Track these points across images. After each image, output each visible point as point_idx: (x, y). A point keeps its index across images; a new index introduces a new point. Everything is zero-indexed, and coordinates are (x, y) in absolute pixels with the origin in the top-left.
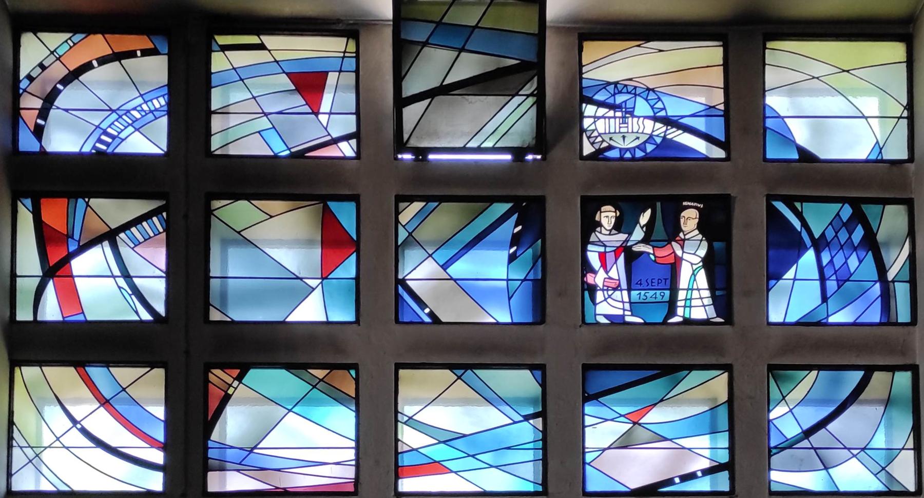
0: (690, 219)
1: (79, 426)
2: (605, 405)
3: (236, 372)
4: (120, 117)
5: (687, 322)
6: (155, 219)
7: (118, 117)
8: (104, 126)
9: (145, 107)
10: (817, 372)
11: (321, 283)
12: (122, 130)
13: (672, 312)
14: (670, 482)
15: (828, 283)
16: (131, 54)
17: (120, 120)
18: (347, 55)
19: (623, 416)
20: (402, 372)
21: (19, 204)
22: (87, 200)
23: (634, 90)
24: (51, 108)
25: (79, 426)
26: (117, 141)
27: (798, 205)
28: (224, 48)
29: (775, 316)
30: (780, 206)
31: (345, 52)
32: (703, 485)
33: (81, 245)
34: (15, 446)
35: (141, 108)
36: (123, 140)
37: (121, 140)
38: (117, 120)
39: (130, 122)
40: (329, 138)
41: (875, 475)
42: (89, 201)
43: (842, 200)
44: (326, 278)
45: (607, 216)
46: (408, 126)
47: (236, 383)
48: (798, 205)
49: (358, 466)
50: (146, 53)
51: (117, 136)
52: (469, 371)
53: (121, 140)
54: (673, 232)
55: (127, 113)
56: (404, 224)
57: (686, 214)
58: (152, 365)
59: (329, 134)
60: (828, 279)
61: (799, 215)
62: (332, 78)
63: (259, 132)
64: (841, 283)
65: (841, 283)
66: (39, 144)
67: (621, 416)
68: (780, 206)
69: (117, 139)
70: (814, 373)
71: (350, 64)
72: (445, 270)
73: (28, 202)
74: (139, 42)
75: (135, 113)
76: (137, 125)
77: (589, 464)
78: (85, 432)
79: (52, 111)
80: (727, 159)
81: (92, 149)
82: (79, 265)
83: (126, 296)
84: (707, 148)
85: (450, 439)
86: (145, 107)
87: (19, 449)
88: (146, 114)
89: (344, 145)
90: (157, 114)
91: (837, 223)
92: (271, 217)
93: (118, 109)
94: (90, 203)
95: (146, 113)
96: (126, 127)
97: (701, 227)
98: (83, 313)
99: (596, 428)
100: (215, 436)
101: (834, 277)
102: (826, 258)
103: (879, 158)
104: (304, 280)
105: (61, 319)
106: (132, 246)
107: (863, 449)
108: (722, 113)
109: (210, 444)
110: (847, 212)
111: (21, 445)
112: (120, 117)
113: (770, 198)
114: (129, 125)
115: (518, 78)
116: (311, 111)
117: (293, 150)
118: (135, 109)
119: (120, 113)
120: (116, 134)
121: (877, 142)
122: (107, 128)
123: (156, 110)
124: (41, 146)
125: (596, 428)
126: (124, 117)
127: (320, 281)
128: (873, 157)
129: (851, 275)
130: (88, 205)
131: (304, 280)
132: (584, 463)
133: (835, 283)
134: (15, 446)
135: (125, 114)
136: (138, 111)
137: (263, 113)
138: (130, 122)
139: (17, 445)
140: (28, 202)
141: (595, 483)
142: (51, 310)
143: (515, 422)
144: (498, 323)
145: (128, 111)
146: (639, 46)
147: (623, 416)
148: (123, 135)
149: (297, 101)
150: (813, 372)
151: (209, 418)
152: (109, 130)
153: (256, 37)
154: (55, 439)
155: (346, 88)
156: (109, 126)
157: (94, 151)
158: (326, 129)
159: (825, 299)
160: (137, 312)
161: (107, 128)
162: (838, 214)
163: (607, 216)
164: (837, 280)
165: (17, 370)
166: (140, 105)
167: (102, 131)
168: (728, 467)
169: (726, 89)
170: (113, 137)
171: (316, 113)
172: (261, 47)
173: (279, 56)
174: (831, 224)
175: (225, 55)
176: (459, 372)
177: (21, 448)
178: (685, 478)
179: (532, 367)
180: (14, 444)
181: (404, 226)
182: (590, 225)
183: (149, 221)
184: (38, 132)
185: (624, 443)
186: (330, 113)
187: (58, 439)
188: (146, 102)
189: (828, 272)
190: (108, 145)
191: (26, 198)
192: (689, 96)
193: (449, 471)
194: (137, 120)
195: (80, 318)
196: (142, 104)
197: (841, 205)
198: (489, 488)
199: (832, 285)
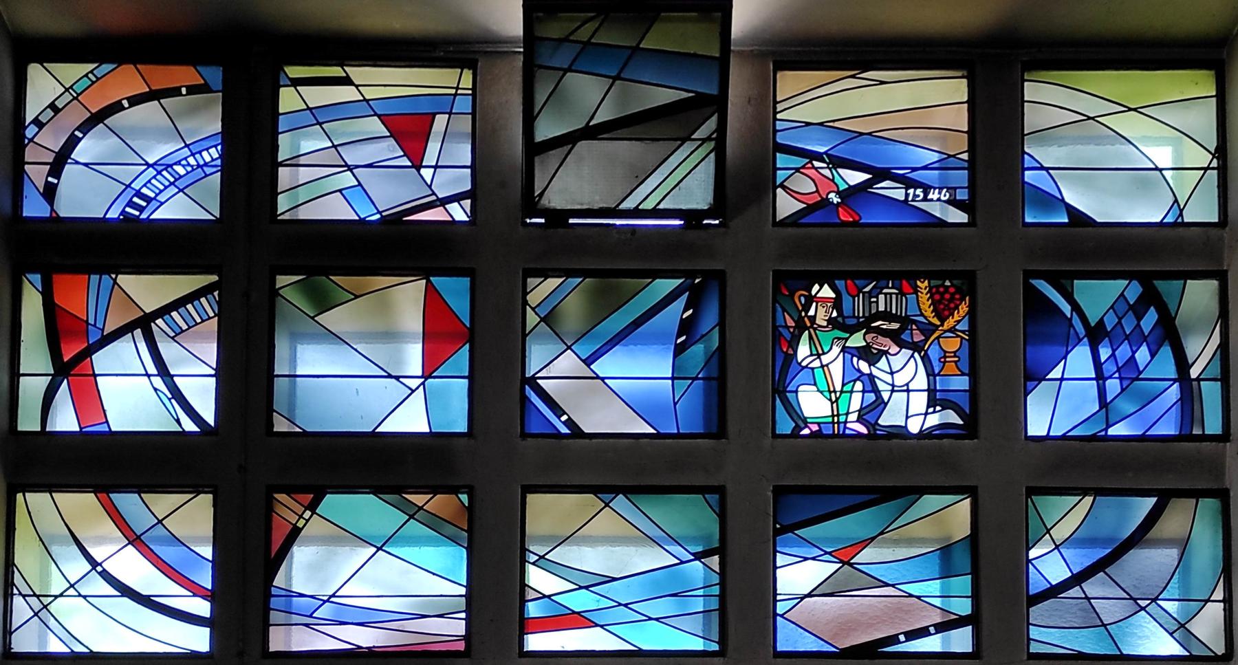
1: (99, 569)
11: (423, 384)
12: (161, 191)
16: (175, 92)
18: (453, 91)
19: (830, 553)
20: (532, 498)
22: (114, 276)
25: (99, 569)
26: (154, 204)
29: (1037, 426)
32: (932, 644)
33: (105, 334)
34: (15, 594)
36: (162, 204)
37: (343, 192)
40: (434, 198)
41: (1171, 634)
44: (430, 377)
47: (308, 514)
53: (343, 192)
59: (434, 194)
62: (440, 121)
63: (340, 191)
74: (186, 75)
76: (179, 183)
77: (782, 616)
78: (107, 576)
81: (121, 214)
87: (21, 598)
88: (193, 170)
90: (208, 170)
93: (155, 163)
96: (166, 187)
98: (107, 422)
100: (279, 581)
106: (172, 334)
109: (274, 591)
111: (23, 593)
118: (178, 163)
120: (152, 195)
121: (1176, 201)
123: (206, 164)
128: (1169, 219)
132: (775, 615)
134: (15, 594)
135: (166, 169)
136: (183, 166)
137: (346, 165)
139: (17, 593)
141: (789, 639)
145: (171, 166)
147: (830, 553)
148: (162, 198)
149: (389, 150)
151: (273, 556)
152: (144, 191)
153: (340, 68)
155: (459, 136)
160: (178, 421)
165: (20, 496)
166: (185, 159)
170: (148, 200)
171: (418, 166)
176: (607, 497)
177: (24, 596)
181: (533, 309)
186: (436, 167)
188: (193, 155)
194: (181, 177)
195: (104, 428)
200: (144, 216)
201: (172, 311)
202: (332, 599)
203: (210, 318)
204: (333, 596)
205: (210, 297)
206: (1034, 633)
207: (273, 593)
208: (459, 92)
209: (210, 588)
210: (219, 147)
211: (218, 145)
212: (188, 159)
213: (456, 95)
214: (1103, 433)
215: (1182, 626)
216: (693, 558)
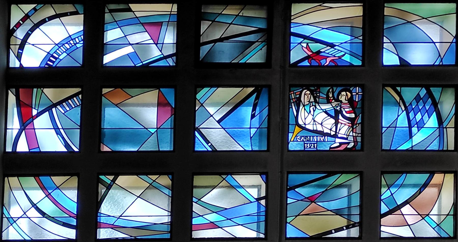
4: (60, 47)
6: (75, 98)
7: (58, 47)
8: (51, 53)
9: (72, 42)
10: (405, 174)
11: (157, 131)
12: (60, 55)
14: (330, 232)
15: (413, 129)
16: (65, 15)
17: (59, 49)
18: (169, 13)
21: (9, 91)
23: (441, 62)
24: (25, 44)
26: (58, 60)
27: (398, 89)
28: (111, 11)
31: (171, 12)
34: (4, 218)
35: (70, 42)
38: (58, 49)
39: (65, 50)
40: (162, 56)
41: (434, 229)
42: (43, 90)
43: (421, 86)
48: (398, 89)
50: (72, 14)
51: (58, 58)
52: (229, 176)
55: (63, 45)
56: (199, 99)
58: (72, 175)
59: (162, 54)
60: (413, 127)
61: (399, 94)
65: (420, 128)
66: (19, 63)
67: (306, 198)
69: (58, 59)
70: (404, 175)
72: (219, 123)
73: (14, 90)
74: (69, 8)
75: (67, 45)
77: (289, 223)
79: (26, 46)
81: (46, 65)
82: (37, 123)
83: (60, 139)
84: (350, 59)
85: (219, 211)
86: (72, 42)
87: (6, 219)
88: (72, 46)
89: (170, 60)
91: (418, 98)
92: (132, 97)
93: (58, 44)
94: (44, 91)
95: (72, 45)
98: (39, 147)
101: (416, 126)
102: (411, 115)
103: (441, 64)
104: (148, 129)
105: (28, 150)
107: (428, 215)
108: (361, 41)
112: (60, 47)
114: (64, 52)
116: (153, 43)
117: (144, 63)
119: (60, 45)
121: (440, 55)
122: (53, 53)
124: (21, 64)
126: (62, 47)
127: (156, 129)
128: (437, 63)
129: (425, 124)
130: (42, 92)
131: (148, 129)
132: (286, 223)
133: (416, 129)
134: (4, 218)
135: (62, 46)
136: (68, 44)
138: (65, 50)
140: (14, 90)
142: (23, 147)
143: (251, 202)
144: (245, 151)
145: (64, 44)
146: (320, 5)
150: (404, 174)
151: (99, 201)
152: (55, 55)
154: (24, 213)
156: (54, 53)
157: (46, 66)
158: (161, 51)
161: (53, 53)
162: (418, 94)
164: (418, 127)
165: (6, 178)
167: (51, 55)
172: (130, 10)
173: (138, 14)
174: (415, 98)
175: (323, 129)
176: (224, 177)
177: (7, 218)
179: (261, 174)
180: (4, 216)
181: (199, 101)
183: (72, 99)
184: (19, 57)
187: (25, 213)
188: (72, 40)
189: (413, 122)
190: (53, 62)
191: (13, 88)
192: (321, 26)
193: (218, 227)
195: (37, 150)
196: (71, 40)
197: (421, 88)
198: (238, 236)
200: (54, 65)
201: (63, 103)
202: (120, 217)
203: (78, 106)
204: (121, 216)
205: (77, 97)
206: (383, 228)
207: (98, 215)
208: (172, 13)
209: (76, 213)
210: (82, 37)
211: (82, 35)
212: (71, 42)
213: (170, 14)
214: (411, 149)
215: (438, 225)
216: (256, 200)
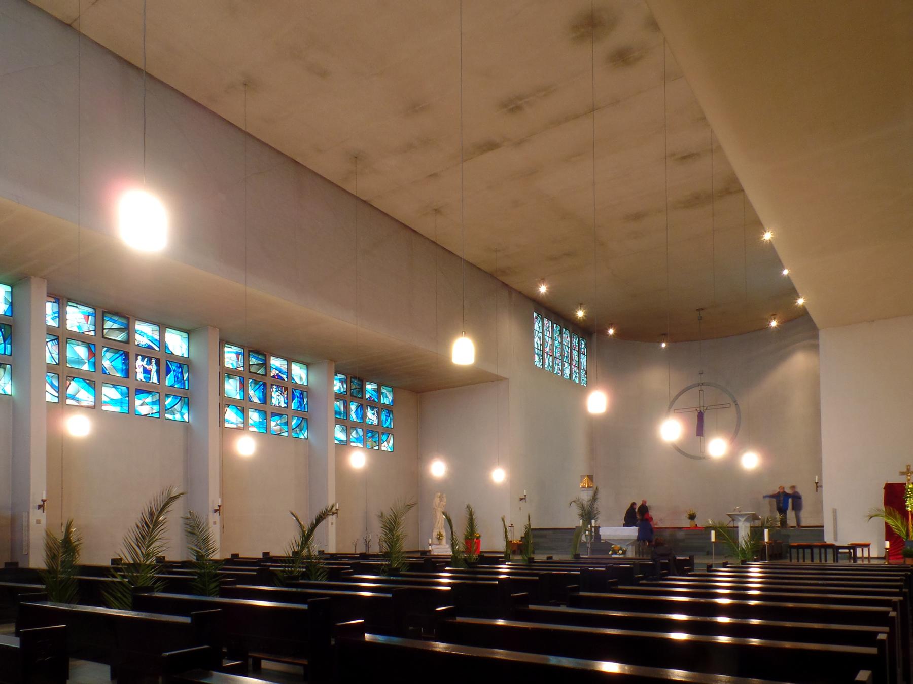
0: (153, 361)
2: (145, 157)
3: (72, 378)
5: (152, 383)
13: (150, 380)
30: (168, 362)
45: (140, 358)
46: (105, 333)
49: (95, 402)
54: (151, 363)
57: (153, 360)
61: (171, 364)
64: (177, 379)
68: (168, 362)
71: (94, 315)
80: (159, 351)
97: (155, 364)
99: (835, 512)
110: (178, 365)
113: (166, 360)
115: (125, 330)
125: (835, 512)
159: (175, 381)
163: (140, 358)
168: (159, 412)
169: (159, 336)
178: (152, 414)
182: (137, 359)
185: (142, 405)
199: (176, 379)
